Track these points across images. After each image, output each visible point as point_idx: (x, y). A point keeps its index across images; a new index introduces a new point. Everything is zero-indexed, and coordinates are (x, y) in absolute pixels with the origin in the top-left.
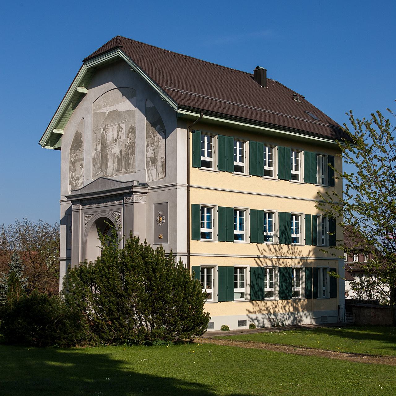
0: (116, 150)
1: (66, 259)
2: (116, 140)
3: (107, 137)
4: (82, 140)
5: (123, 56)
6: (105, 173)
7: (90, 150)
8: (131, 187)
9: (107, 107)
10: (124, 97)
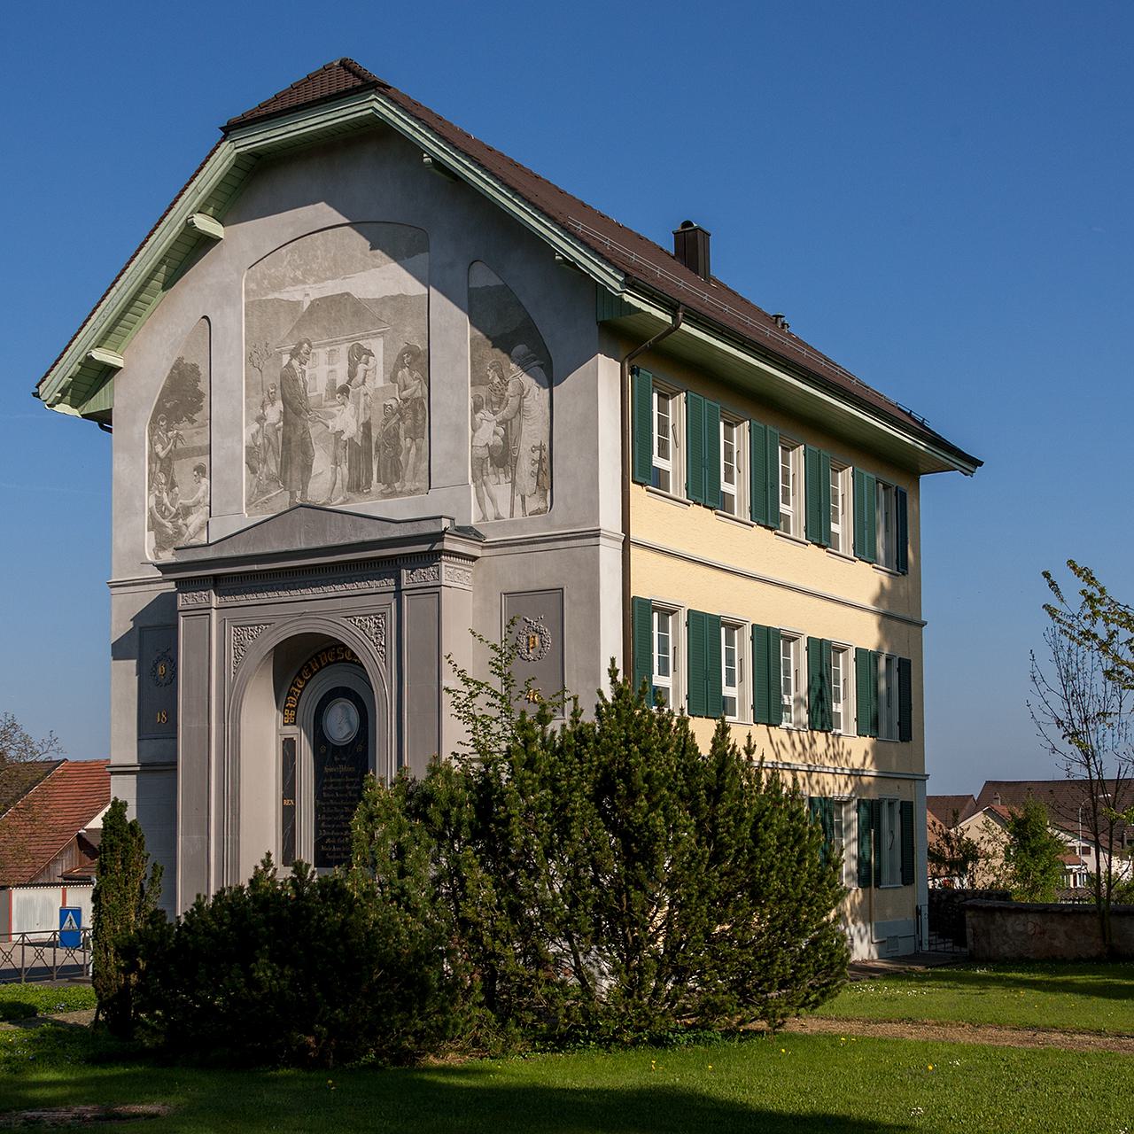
0: (346, 420)
1: (138, 768)
2: (344, 390)
3: (307, 378)
4: (203, 386)
5: (391, 116)
6: (299, 493)
7: (237, 418)
8: (439, 537)
9: (305, 283)
10: (378, 251)
